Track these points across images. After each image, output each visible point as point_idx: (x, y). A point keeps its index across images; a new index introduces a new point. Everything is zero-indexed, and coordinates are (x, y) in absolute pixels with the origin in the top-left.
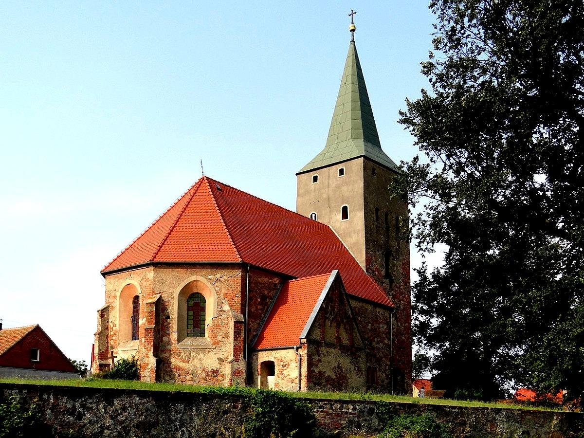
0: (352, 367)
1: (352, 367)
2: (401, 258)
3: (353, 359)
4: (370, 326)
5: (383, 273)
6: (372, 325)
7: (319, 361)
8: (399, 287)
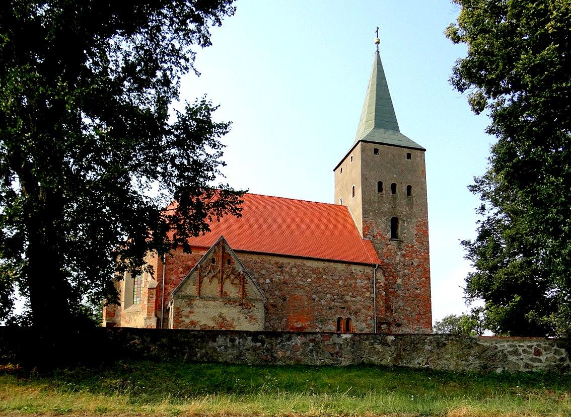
0: (242, 316)
1: (241, 316)
2: (414, 221)
3: (243, 309)
4: (341, 283)
5: (389, 236)
6: (345, 280)
7: (191, 312)
8: (412, 246)
